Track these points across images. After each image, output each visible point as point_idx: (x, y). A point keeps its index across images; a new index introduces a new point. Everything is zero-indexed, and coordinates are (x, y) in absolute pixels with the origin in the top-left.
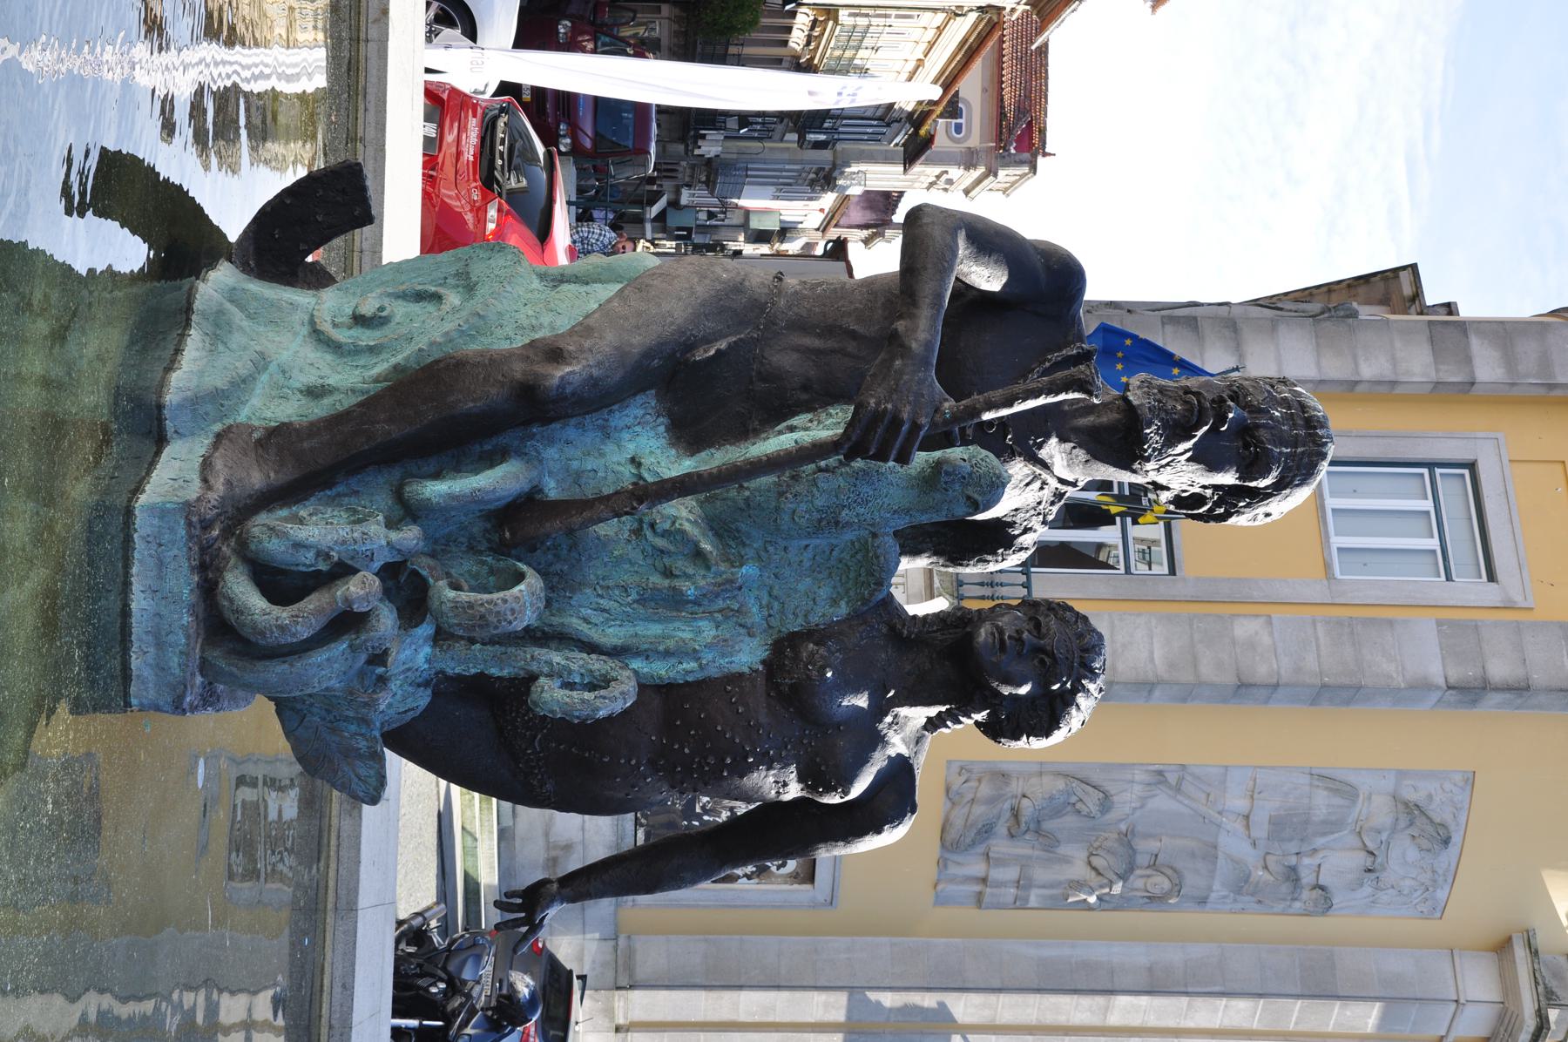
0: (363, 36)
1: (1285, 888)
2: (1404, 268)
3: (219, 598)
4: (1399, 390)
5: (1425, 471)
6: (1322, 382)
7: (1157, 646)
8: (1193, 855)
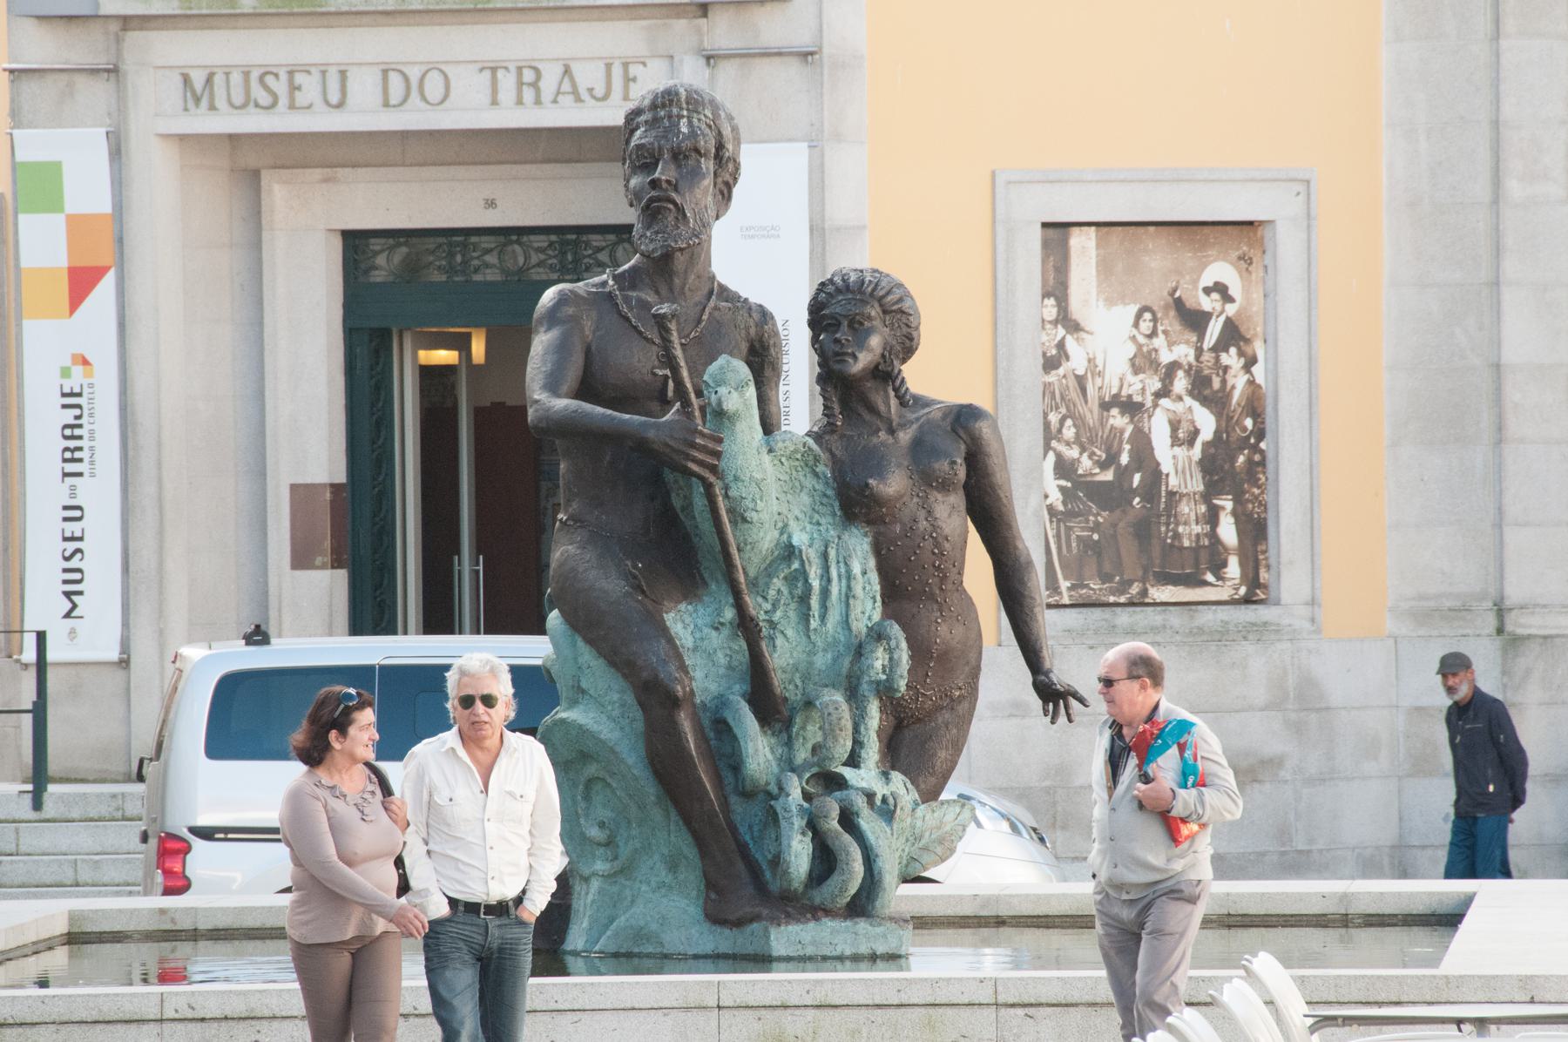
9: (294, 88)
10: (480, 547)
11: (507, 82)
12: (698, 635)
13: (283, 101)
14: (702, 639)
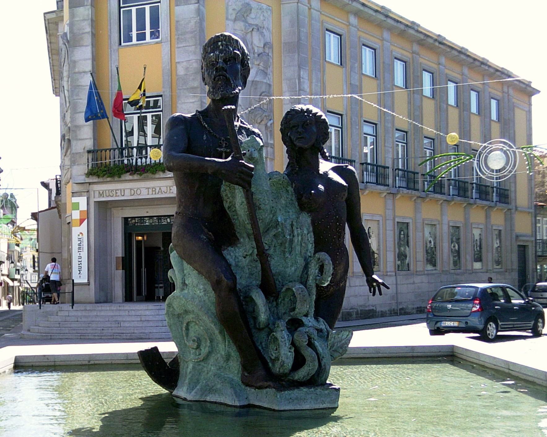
0: (53, 364)
1: (265, 58)
2: (45, 17)
3: (303, 380)
4: (94, 19)
5: (122, 10)
6: (92, 45)
7: (188, 101)
8: (256, 89)
9: (116, 193)
10: (145, 267)
11: (150, 190)
12: (237, 260)
13: (115, 195)
14: (238, 262)
